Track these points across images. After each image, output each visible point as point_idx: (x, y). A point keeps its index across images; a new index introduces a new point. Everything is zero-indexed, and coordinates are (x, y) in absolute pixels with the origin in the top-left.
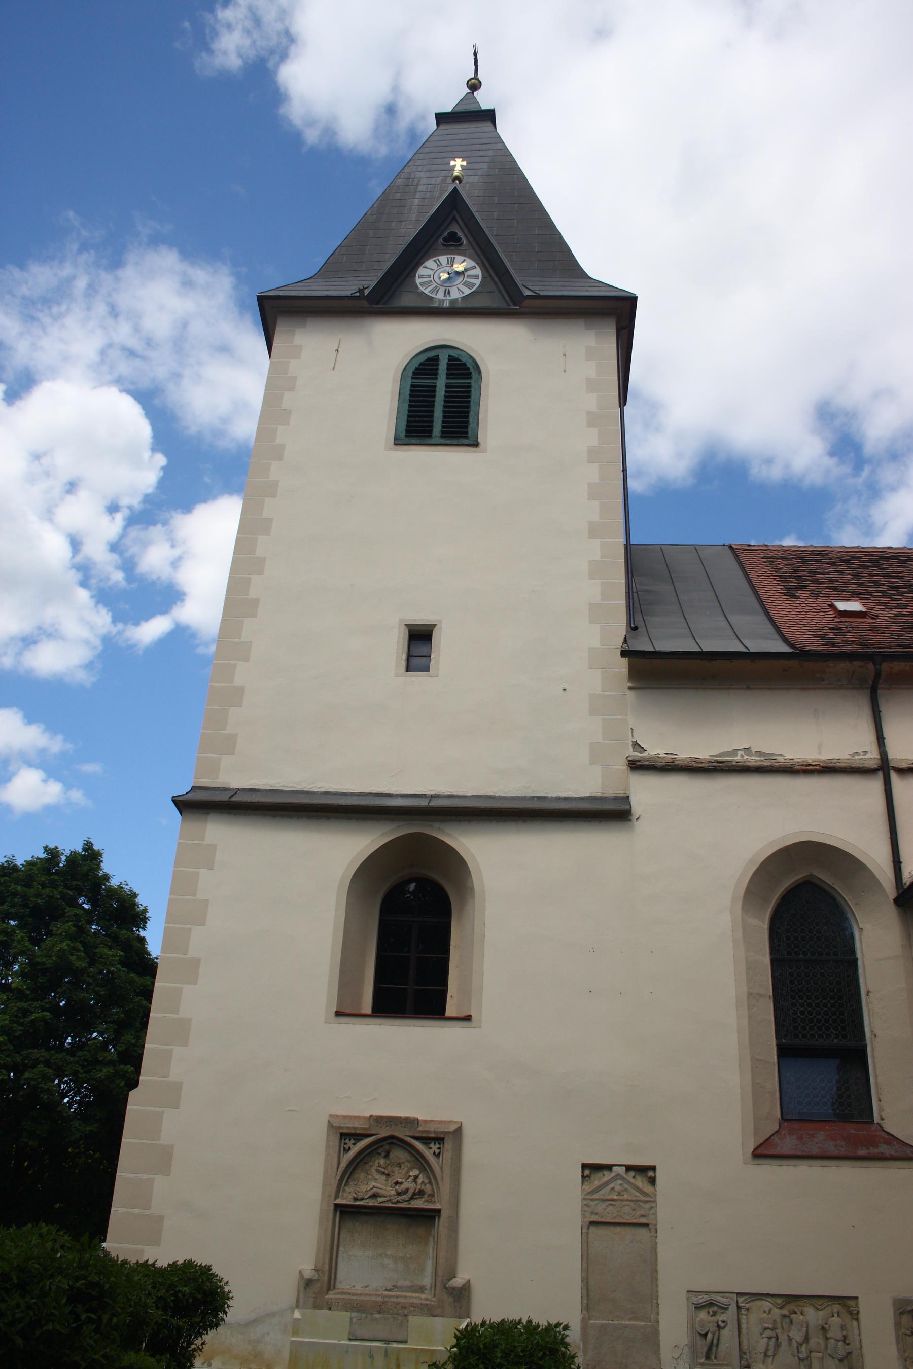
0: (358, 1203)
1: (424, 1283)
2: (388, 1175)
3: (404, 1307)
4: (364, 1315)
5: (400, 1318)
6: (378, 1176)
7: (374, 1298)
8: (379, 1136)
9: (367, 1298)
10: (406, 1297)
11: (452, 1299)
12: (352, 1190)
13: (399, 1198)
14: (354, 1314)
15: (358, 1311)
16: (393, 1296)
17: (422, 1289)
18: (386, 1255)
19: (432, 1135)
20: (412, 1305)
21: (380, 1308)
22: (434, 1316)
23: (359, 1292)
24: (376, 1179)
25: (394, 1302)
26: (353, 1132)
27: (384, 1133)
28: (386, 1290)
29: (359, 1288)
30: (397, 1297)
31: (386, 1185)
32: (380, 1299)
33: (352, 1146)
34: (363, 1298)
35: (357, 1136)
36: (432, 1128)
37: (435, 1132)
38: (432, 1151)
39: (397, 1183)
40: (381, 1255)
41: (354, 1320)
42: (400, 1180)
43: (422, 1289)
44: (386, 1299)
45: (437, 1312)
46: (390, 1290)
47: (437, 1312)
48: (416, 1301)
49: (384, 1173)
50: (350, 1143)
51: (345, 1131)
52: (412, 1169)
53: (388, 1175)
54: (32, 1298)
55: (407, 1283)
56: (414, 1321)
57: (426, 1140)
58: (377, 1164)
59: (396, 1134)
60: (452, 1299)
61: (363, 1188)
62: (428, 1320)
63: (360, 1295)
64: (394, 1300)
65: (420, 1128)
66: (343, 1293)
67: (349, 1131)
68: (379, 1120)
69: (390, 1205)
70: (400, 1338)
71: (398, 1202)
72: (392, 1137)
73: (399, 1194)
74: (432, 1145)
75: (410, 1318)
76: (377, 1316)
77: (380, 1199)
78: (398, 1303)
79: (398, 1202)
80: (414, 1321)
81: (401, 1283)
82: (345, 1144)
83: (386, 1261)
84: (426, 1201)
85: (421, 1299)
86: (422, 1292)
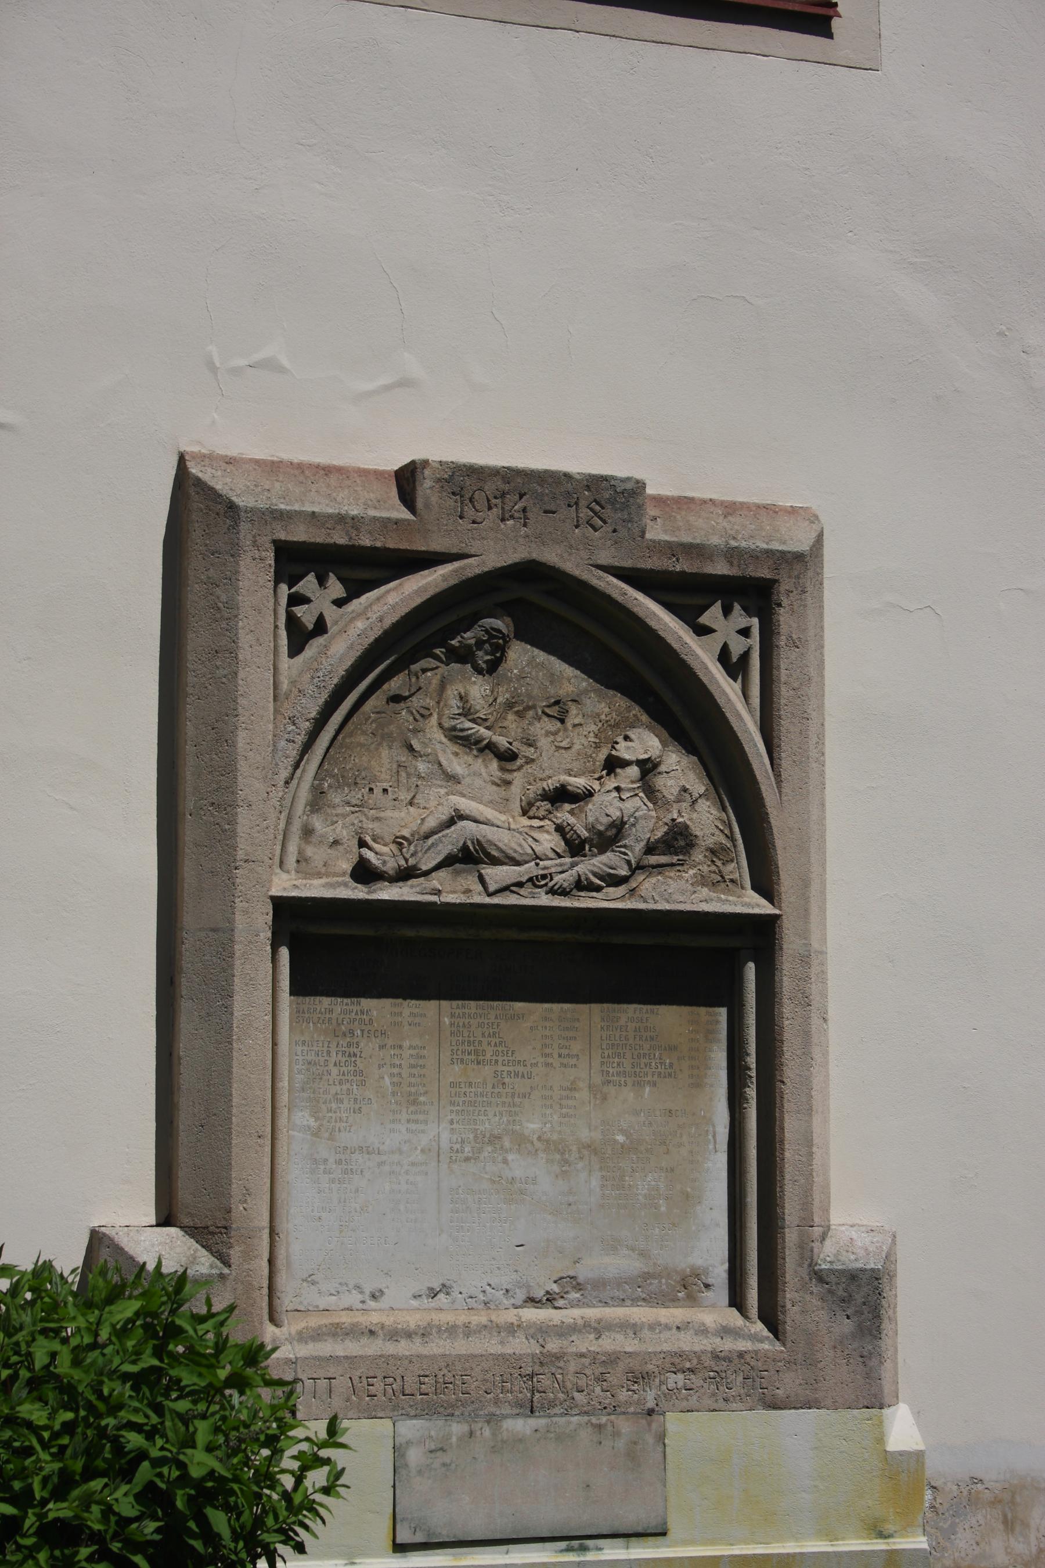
0: (387, 893)
1: (697, 1259)
2: (507, 757)
3: (639, 1378)
4: (457, 1429)
5: (625, 1426)
6: (457, 762)
7: (492, 1346)
8: (472, 567)
9: (461, 1346)
10: (634, 1329)
11: (847, 1326)
12: (343, 831)
13: (589, 866)
14: (410, 1428)
15: (428, 1411)
16: (573, 1329)
17: (688, 1286)
18: (521, 1141)
19: (720, 568)
20: (679, 1363)
21: (534, 1386)
22: (774, 1405)
23: (412, 1321)
24: (452, 778)
25: (594, 1357)
26: (340, 539)
27: (494, 549)
28: (532, 1301)
29: (402, 1305)
30: (599, 1329)
31: (502, 805)
32: (520, 1346)
33: (331, 614)
34: (438, 1347)
35: (363, 566)
36: (708, 531)
37: (732, 554)
38: (715, 643)
39: (561, 795)
40: (494, 1139)
41: (414, 1456)
42: (579, 782)
43: (688, 1286)
44: (553, 1345)
45: (789, 1383)
46: (550, 1300)
47: (789, 1383)
48: (687, 1342)
49: (491, 747)
50: (322, 596)
51: (300, 534)
52: (622, 727)
53: (507, 757)
54: (770, 525)
55: (621, 1264)
56: (689, 1431)
57: (689, 592)
58: (454, 704)
59: (551, 556)
60: (847, 1326)
61: (404, 820)
62: (746, 1428)
63: (425, 1333)
64: (585, 1343)
65: (656, 533)
66: (338, 1332)
67: (318, 537)
68: (467, 483)
69: (544, 900)
70: (631, 1517)
71: (581, 885)
72: (530, 573)
73: (576, 847)
74: (713, 615)
75: (673, 1422)
76: (520, 1426)
77: (497, 875)
78: (613, 1359)
79: (581, 885)
80: (689, 1431)
81: (598, 1264)
82: (296, 600)
83: (519, 1166)
84: (703, 881)
85: (703, 1331)
86: (692, 1300)
